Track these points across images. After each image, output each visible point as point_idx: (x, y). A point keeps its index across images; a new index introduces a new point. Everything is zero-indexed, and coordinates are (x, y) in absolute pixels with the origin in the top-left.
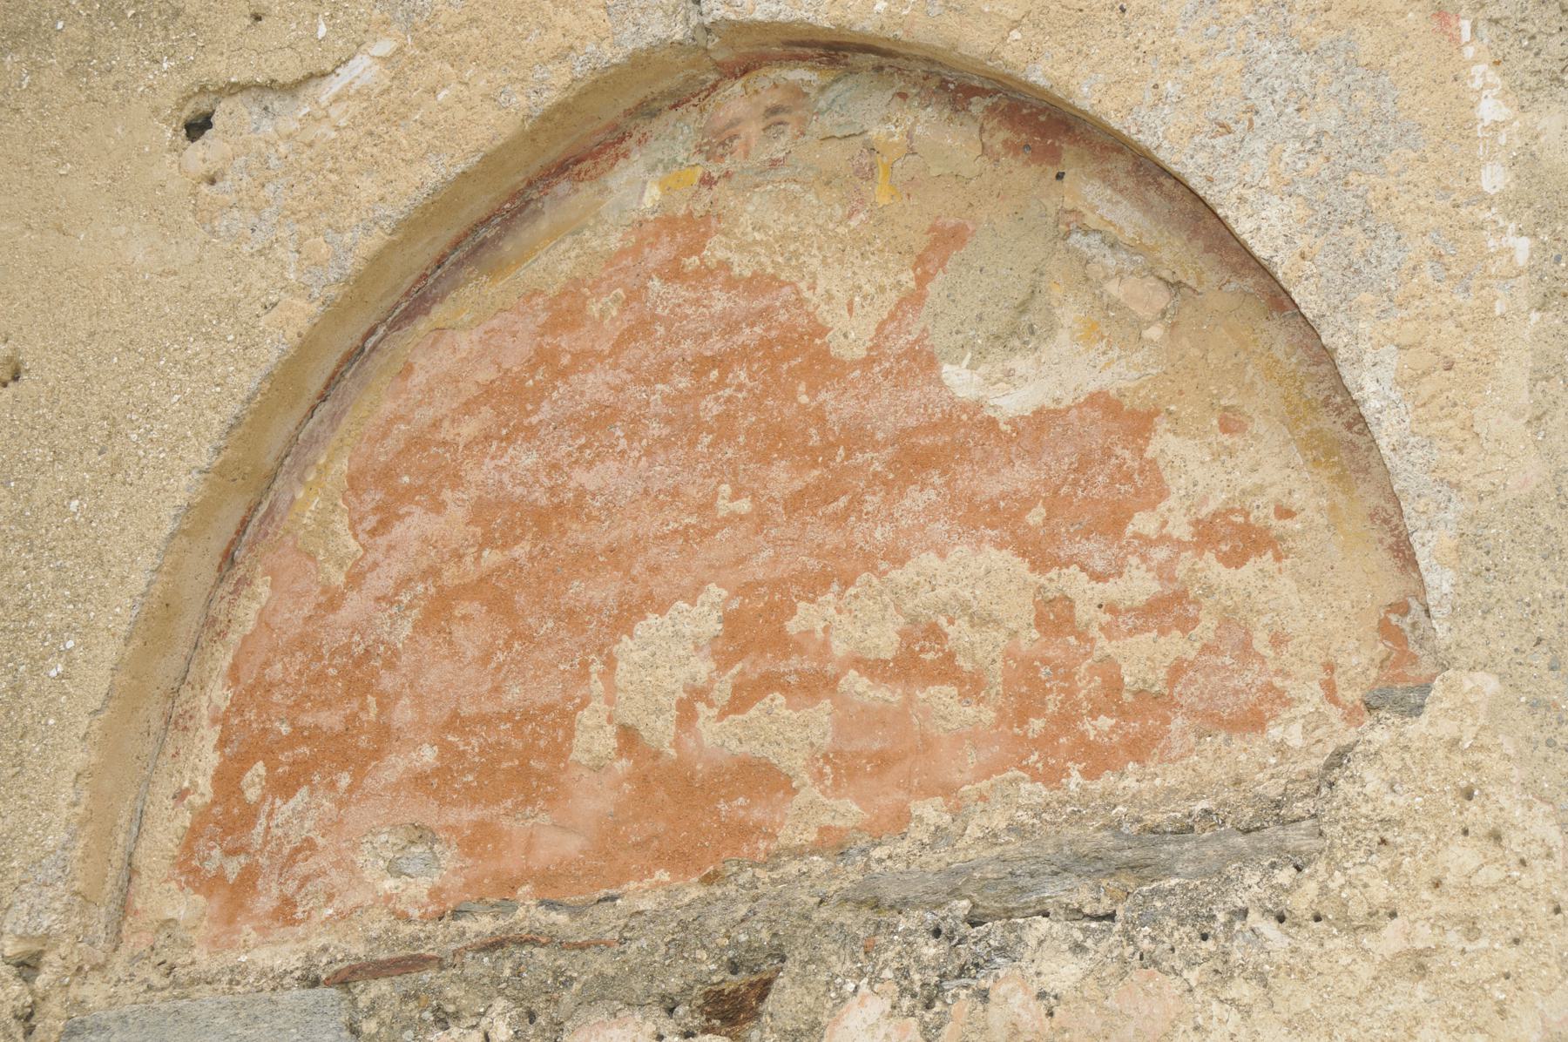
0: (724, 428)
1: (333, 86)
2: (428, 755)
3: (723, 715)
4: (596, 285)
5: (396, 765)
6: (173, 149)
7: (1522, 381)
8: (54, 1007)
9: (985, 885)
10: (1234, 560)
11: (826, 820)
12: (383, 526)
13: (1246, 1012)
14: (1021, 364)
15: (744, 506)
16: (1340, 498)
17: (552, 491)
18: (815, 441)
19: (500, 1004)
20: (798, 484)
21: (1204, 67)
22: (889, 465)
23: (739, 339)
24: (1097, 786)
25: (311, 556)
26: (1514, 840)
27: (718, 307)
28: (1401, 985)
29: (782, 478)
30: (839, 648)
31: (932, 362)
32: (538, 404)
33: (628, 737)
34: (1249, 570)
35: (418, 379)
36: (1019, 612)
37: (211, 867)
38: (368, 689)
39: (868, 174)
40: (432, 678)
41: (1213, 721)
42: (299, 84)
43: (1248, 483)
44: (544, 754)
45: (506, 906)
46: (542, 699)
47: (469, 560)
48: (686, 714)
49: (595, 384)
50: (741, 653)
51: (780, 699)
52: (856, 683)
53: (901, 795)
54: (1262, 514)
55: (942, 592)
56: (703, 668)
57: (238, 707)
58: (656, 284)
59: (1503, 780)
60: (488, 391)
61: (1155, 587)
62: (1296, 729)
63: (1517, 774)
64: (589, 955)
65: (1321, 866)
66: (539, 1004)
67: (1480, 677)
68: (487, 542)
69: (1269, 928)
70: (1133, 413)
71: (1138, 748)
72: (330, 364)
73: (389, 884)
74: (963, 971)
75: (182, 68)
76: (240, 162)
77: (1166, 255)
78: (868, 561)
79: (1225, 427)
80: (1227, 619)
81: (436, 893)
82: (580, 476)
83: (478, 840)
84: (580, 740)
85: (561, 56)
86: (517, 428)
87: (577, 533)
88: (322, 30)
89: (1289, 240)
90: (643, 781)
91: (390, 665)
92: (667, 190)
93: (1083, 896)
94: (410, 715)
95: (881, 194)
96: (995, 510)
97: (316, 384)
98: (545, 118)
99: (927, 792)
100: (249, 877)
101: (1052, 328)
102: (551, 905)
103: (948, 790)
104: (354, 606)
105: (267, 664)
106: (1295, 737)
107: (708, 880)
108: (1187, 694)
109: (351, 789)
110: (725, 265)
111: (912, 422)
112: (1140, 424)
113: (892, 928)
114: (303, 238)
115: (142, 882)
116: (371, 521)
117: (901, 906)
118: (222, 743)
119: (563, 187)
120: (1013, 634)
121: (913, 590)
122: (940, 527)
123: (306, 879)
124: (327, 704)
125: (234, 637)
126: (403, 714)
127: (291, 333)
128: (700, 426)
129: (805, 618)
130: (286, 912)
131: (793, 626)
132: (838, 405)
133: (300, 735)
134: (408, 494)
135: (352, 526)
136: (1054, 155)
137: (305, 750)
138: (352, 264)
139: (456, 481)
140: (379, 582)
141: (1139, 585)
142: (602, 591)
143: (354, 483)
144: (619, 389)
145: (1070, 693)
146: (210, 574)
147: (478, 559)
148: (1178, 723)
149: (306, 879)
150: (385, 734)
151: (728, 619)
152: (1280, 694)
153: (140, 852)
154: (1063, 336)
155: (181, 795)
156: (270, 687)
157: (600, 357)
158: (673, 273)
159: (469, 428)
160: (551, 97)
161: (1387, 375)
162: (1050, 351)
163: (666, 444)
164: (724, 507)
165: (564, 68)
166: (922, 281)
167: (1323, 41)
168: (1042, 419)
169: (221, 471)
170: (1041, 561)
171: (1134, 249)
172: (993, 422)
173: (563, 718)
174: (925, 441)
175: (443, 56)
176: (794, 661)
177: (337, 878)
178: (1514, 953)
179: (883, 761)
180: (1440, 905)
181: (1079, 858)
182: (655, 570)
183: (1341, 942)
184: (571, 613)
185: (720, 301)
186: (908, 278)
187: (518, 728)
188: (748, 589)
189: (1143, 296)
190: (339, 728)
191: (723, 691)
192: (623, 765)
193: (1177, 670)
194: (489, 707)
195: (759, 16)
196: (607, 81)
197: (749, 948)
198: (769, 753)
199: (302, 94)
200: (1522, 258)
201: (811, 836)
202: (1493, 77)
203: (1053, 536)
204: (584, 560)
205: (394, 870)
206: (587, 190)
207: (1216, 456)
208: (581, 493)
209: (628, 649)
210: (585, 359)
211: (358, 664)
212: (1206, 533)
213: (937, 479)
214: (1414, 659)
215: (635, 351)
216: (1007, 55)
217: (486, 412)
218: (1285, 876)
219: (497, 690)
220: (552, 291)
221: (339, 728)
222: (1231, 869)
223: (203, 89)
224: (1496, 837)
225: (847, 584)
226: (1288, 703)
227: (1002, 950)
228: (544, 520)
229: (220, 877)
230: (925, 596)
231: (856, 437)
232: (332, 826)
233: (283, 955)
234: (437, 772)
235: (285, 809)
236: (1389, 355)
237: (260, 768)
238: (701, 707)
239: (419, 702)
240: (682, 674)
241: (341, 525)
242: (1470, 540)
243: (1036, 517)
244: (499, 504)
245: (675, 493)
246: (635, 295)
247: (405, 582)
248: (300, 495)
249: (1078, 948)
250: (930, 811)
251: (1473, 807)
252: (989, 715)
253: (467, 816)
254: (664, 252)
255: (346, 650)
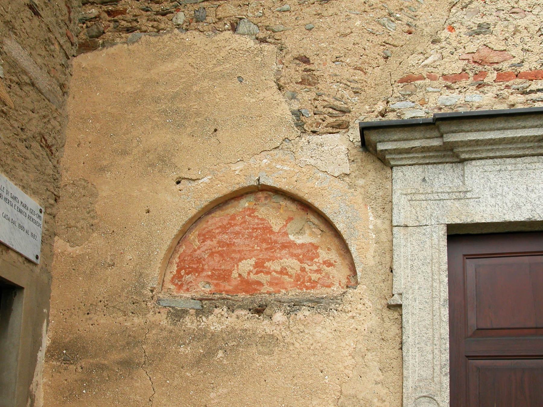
0: (256, 238)
1: (200, 181)
2: (210, 273)
3: (254, 275)
4: (238, 215)
5: (205, 274)
6: (175, 185)
7: (373, 252)
8: (155, 296)
9: (296, 301)
10: (328, 266)
11: (268, 290)
12: (203, 242)
13: (331, 320)
14: (300, 237)
15: (259, 248)
16: (343, 261)
17: (230, 241)
18: (270, 241)
19: (225, 306)
20: (267, 247)
21: (333, 205)
22: (280, 247)
23: (259, 226)
24: (308, 291)
25: (192, 244)
26: (366, 305)
27: (256, 222)
28: (351, 320)
29: (264, 245)
30: (272, 269)
31: (287, 234)
32: (228, 229)
33: (240, 275)
34: (330, 268)
35: (209, 223)
36: (298, 268)
37: (176, 282)
38: (200, 263)
39: (280, 208)
40: (211, 263)
41: (323, 286)
42: (195, 180)
43: (331, 257)
44: (227, 276)
45: (221, 294)
46: (227, 268)
47: (217, 249)
48: (249, 274)
49: (237, 228)
50: (257, 267)
51: (263, 274)
52: (274, 273)
53: (279, 288)
54: (332, 261)
55: (287, 264)
56: (252, 268)
57: (180, 262)
58: (247, 216)
59: (366, 298)
60: (220, 227)
61: (317, 268)
62: (335, 288)
63: (367, 298)
64: (238, 302)
65: (342, 305)
66: (231, 307)
67: (364, 286)
68: (220, 246)
69: (335, 311)
70: (316, 246)
71: (313, 287)
72: (196, 219)
73: (203, 289)
74: (293, 311)
75: (177, 174)
76: (185, 189)
77: (321, 227)
78: (277, 258)
79: (328, 250)
80: (326, 274)
81: (210, 291)
82: (234, 240)
83: (216, 285)
84: (233, 275)
85: (238, 184)
86: (225, 232)
87: (233, 248)
88: (200, 173)
89: (343, 229)
90: (242, 281)
91: (204, 260)
92: (249, 204)
93: (310, 304)
94: (207, 267)
95: (281, 211)
96: (295, 255)
97: (194, 221)
98: (234, 192)
99: (283, 289)
100: (182, 285)
101: (305, 233)
102: (228, 295)
103: (286, 289)
104: (198, 252)
105: (185, 257)
106: (335, 289)
107: (251, 295)
108: (320, 282)
109: (198, 276)
110: (257, 216)
111: (284, 242)
112: (316, 248)
113: (283, 305)
114: (195, 201)
115: (165, 282)
116: (202, 241)
117: (284, 302)
118: (177, 267)
119: (233, 201)
120: (297, 271)
121: (283, 263)
122: (287, 256)
123: (191, 286)
124: (194, 264)
125: (179, 253)
126: (206, 267)
127: (193, 214)
128: (253, 237)
129: (267, 264)
130: (188, 290)
131: (265, 265)
132: (274, 238)
133: (189, 267)
134: (208, 238)
135: (198, 241)
136: (307, 211)
137: (191, 269)
138: (203, 206)
139: (215, 237)
140: (202, 249)
141: (315, 267)
142: (237, 256)
143: (199, 235)
144: (241, 230)
145: (304, 279)
146: (176, 244)
147: (218, 249)
148: (319, 285)
149: (191, 286)
150: (203, 270)
151: (255, 262)
152: (333, 284)
153: (165, 279)
154: (306, 234)
155: (171, 272)
156: (185, 260)
157: (238, 225)
158: (250, 216)
159: (217, 231)
160: (235, 189)
161: (355, 248)
162: (304, 236)
163: (247, 238)
164: (256, 248)
165: (238, 185)
166: (287, 223)
167: (350, 205)
168: (303, 245)
169: (181, 231)
170: (301, 263)
171: (316, 225)
172: (296, 244)
173: (231, 272)
174: (286, 244)
175: (219, 180)
176: (265, 269)
177: (196, 287)
178: (365, 317)
179: (277, 284)
180: (357, 311)
181: (309, 300)
182: (245, 254)
183: (345, 314)
184: (232, 258)
185: (256, 221)
186: (285, 223)
187: (223, 272)
188: (259, 259)
189: (318, 232)
190: (196, 267)
191: (255, 271)
192: (239, 279)
193: (319, 279)
194: (219, 268)
195: (268, 184)
196: (244, 188)
197: (262, 304)
198: (261, 280)
199: (196, 181)
200: (374, 237)
201: (266, 292)
202: (372, 214)
203: (303, 260)
204: (234, 251)
205: (204, 287)
206: (236, 202)
207: (327, 253)
208: (234, 242)
209: (240, 264)
210: (235, 225)
211: (199, 259)
212: (324, 263)
213: (287, 249)
214: (351, 282)
215: (244, 225)
216: (305, 197)
217: (220, 229)
218: (337, 306)
219: (220, 266)
220: (231, 215)
221: (196, 267)
222: (330, 304)
223: (180, 178)
224: (364, 304)
225: (273, 261)
226: (334, 285)
227: (298, 309)
228: (228, 245)
229: (177, 284)
230: (285, 264)
231: (276, 242)
232: (195, 280)
233: (188, 295)
234: (211, 275)
235: (187, 277)
236: (355, 245)
237: (184, 271)
238: (251, 273)
239: (208, 266)
240: (249, 268)
241: (197, 241)
242: (364, 270)
243: (301, 257)
244: (221, 242)
245: (248, 245)
246: (244, 217)
247: (207, 250)
248: (190, 235)
249: (309, 310)
250: (284, 291)
251: (361, 301)
252: (292, 280)
253: (215, 282)
254: (248, 212)
255: (197, 257)
